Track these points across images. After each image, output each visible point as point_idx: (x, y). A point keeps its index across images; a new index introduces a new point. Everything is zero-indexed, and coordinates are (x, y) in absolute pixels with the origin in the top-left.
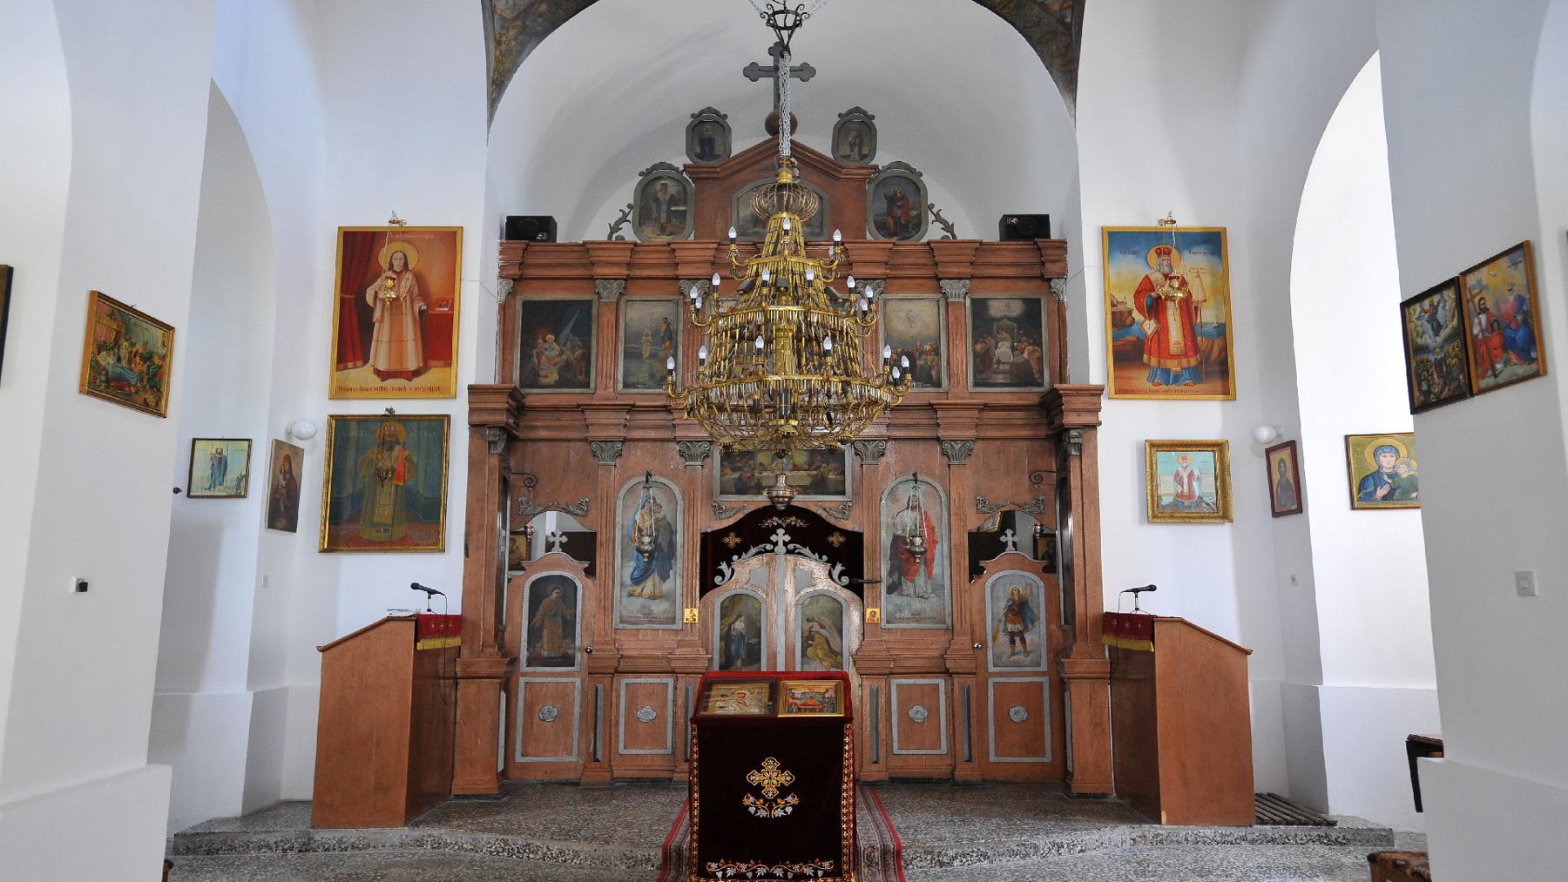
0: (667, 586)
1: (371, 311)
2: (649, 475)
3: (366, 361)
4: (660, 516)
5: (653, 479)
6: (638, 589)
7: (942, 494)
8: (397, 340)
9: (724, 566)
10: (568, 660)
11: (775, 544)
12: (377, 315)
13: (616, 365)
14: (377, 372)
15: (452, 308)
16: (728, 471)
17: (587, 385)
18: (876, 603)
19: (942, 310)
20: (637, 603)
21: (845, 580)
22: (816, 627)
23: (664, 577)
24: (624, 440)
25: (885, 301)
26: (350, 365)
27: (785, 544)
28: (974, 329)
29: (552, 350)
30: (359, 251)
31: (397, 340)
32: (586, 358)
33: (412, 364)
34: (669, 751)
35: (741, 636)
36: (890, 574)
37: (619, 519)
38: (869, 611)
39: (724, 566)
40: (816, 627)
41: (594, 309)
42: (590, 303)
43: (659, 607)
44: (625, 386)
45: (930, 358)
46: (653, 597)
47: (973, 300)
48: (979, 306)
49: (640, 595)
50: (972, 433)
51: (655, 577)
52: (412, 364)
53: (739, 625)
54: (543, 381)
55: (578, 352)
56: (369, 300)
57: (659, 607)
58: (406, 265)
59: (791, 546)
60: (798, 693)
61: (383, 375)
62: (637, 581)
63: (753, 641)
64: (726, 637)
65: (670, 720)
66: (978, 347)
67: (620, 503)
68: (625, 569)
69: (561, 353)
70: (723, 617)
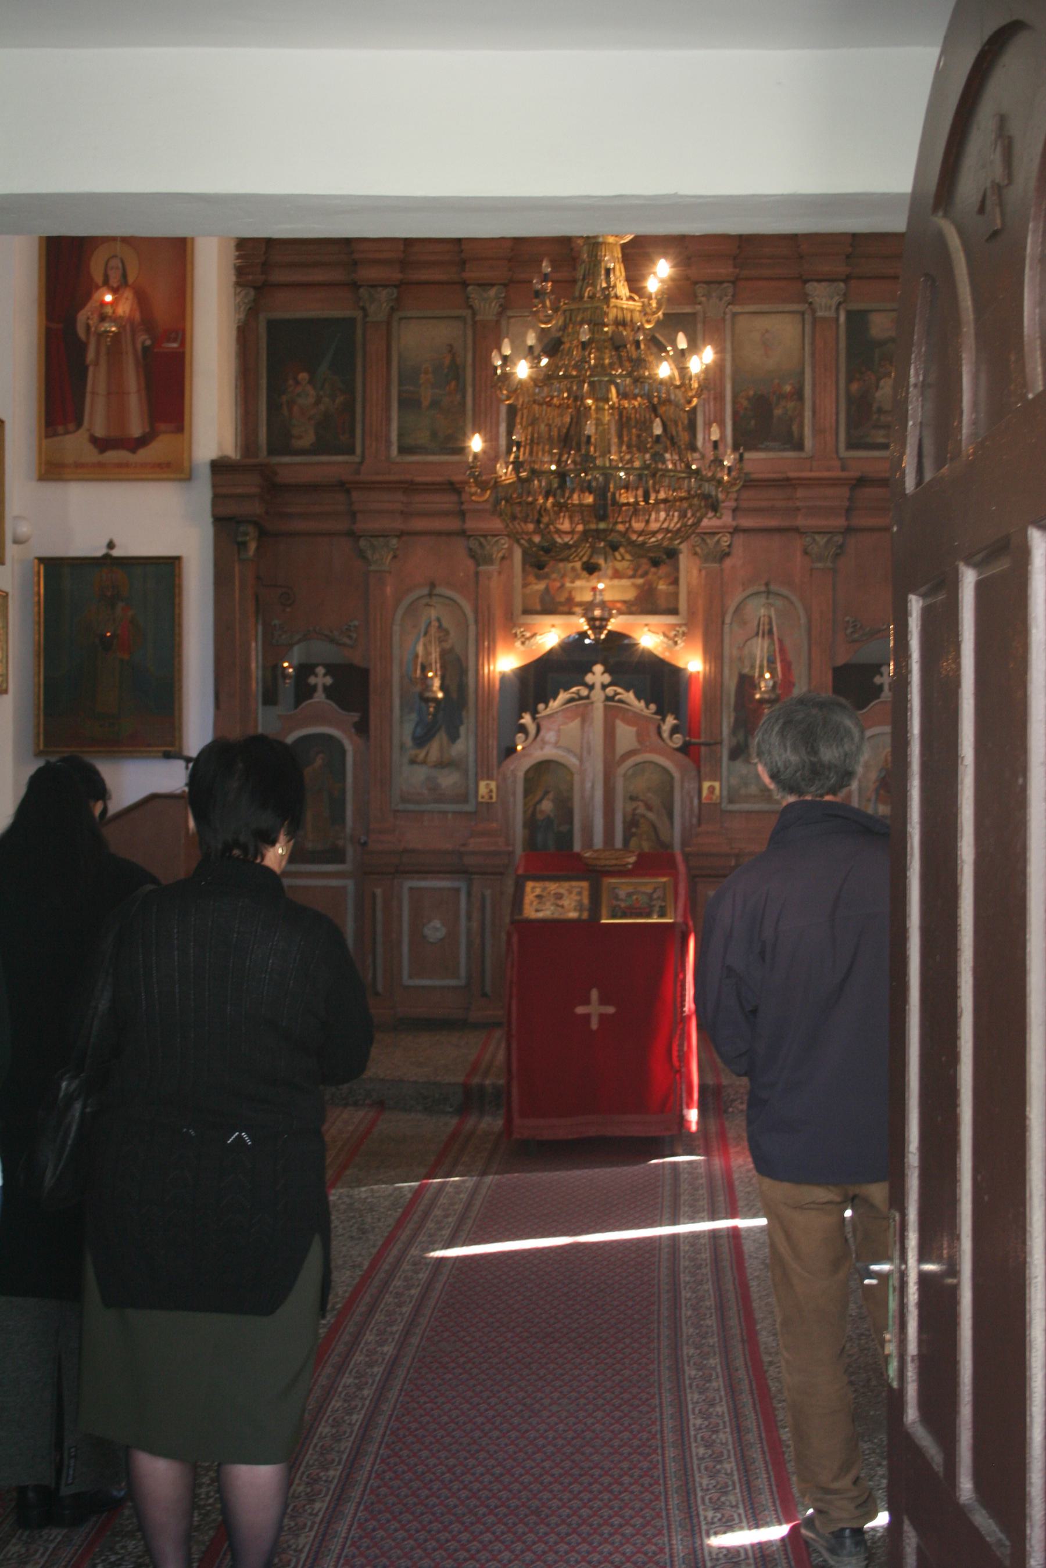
0: (459, 747)
1: (83, 347)
2: (433, 585)
3: (79, 424)
4: (447, 646)
5: (439, 590)
6: (422, 755)
7: (802, 612)
8: (116, 393)
9: (527, 719)
10: (336, 855)
11: (591, 687)
12: (91, 355)
13: (389, 420)
14: (94, 440)
15: (183, 344)
16: (531, 579)
17: (351, 451)
18: (715, 776)
19: (808, 328)
20: (420, 774)
21: (678, 739)
22: (642, 810)
23: (454, 737)
24: (401, 534)
25: (735, 315)
26: (60, 429)
27: (604, 687)
28: (850, 356)
29: (306, 396)
30: (67, 264)
31: (116, 393)
32: (349, 407)
33: (136, 428)
34: (462, 982)
35: (549, 820)
36: (734, 732)
37: (396, 652)
38: (706, 785)
39: (527, 719)
40: (642, 810)
41: (359, 332)
42: (352, 321)
43: (448, 780)
44: (403, 450)
45: (791, 405)
46: (442, 764)
47: (849, 313)
48: (857, 321)
49: (424, 762)
50: (840, 522)
51: (442, 737)
52: (136, 428)
53: (547, 806)
54: (298, 444)
55: (340, 399)
56: (81, 333)
57: (448, 780)
58: (125, 276)
59: (610, 691)
60: (622, 894)
61: (102, 444)
62: (421, 741)
63: (564, 828)
64: (531, 823)
65: (463, 940)
66: (855, 387)
67: (396, 628)
68: (404, 730)
69: (318, 402)
70: (527, 792)
